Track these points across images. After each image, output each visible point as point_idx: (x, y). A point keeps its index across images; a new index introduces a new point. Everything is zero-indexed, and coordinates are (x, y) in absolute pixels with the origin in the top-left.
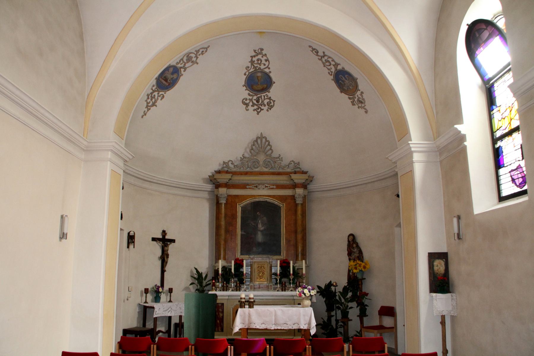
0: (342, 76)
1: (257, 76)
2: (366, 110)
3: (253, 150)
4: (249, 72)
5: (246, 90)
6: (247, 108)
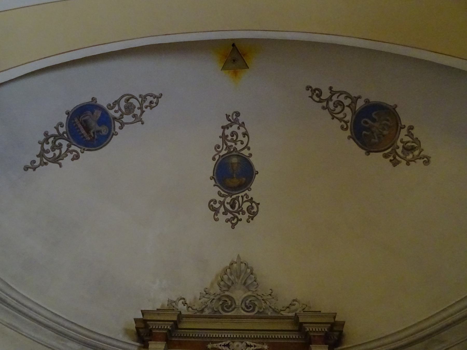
0: (367, 120)
1: (232, 164)
2: (425, 159)
3: (223, 281)
4: (219, 155)
5: (214, 186)
6: (216, 217)
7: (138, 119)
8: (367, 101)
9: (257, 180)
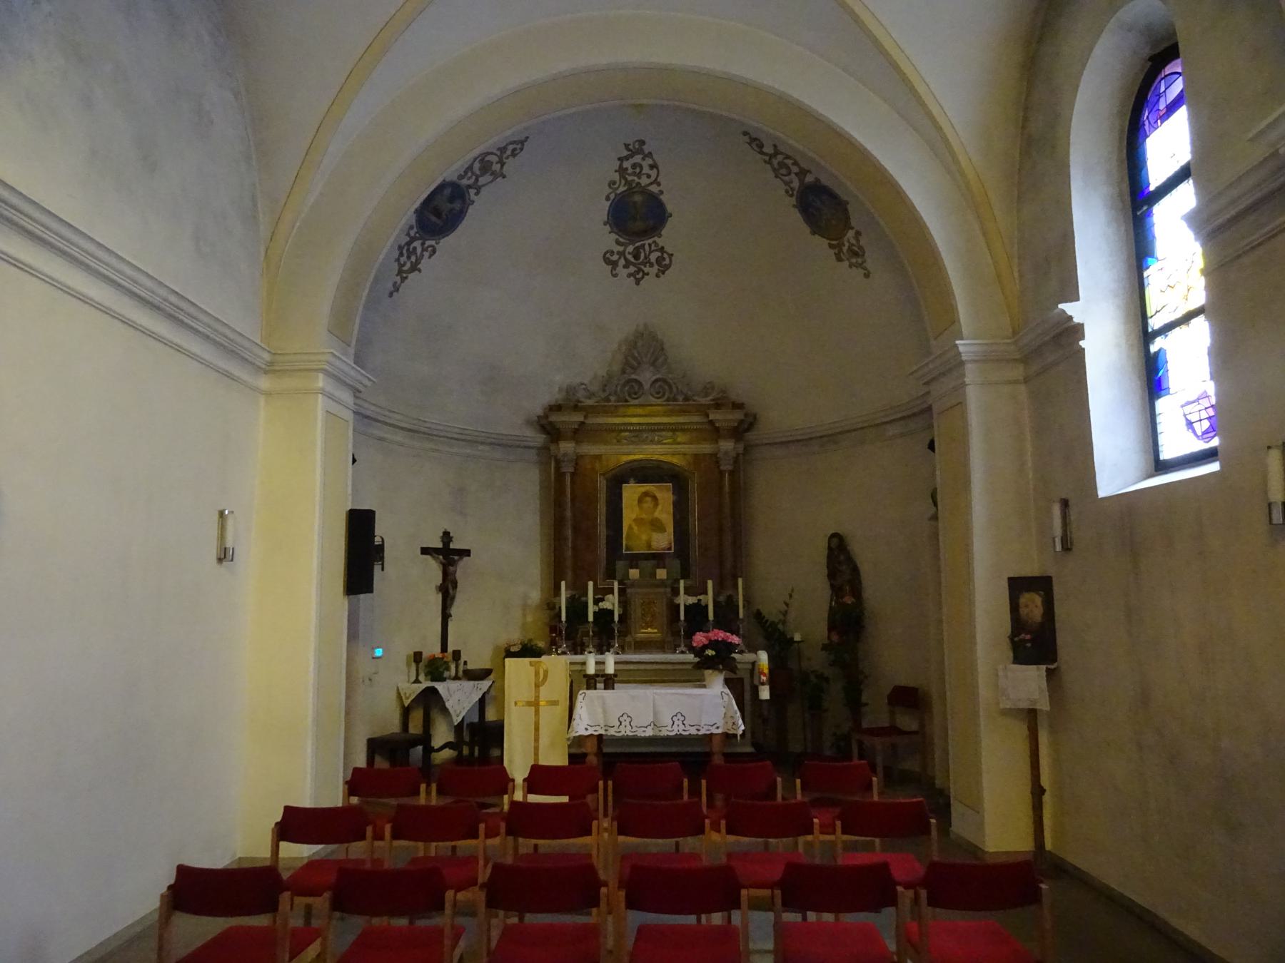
6: (614, 272)
7: (496, 175)
8: (817, 180)
9: (670, 223)
